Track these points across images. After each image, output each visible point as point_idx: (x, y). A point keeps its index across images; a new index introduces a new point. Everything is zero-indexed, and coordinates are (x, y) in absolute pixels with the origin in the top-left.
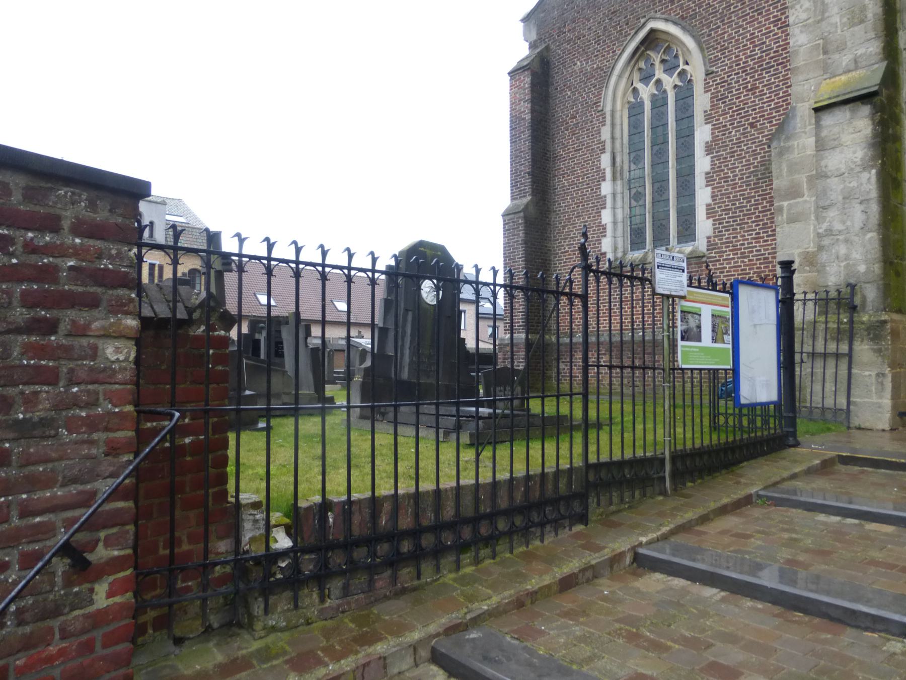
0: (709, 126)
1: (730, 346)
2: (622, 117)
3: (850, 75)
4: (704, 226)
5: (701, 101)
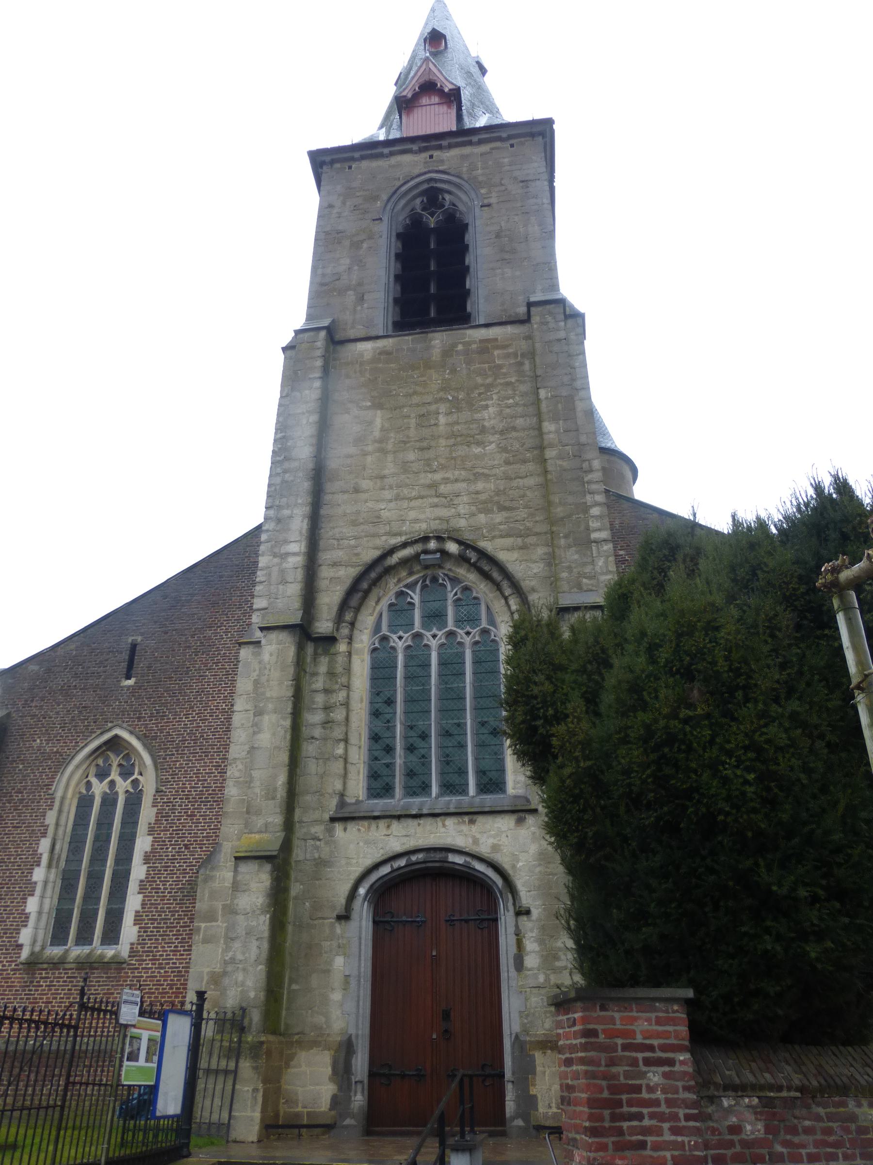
0: (150, 838)
1: (155, 1065)
2: (70, 805)
3: (262, 836)
4: (129, 931)
5: (147, 814)
